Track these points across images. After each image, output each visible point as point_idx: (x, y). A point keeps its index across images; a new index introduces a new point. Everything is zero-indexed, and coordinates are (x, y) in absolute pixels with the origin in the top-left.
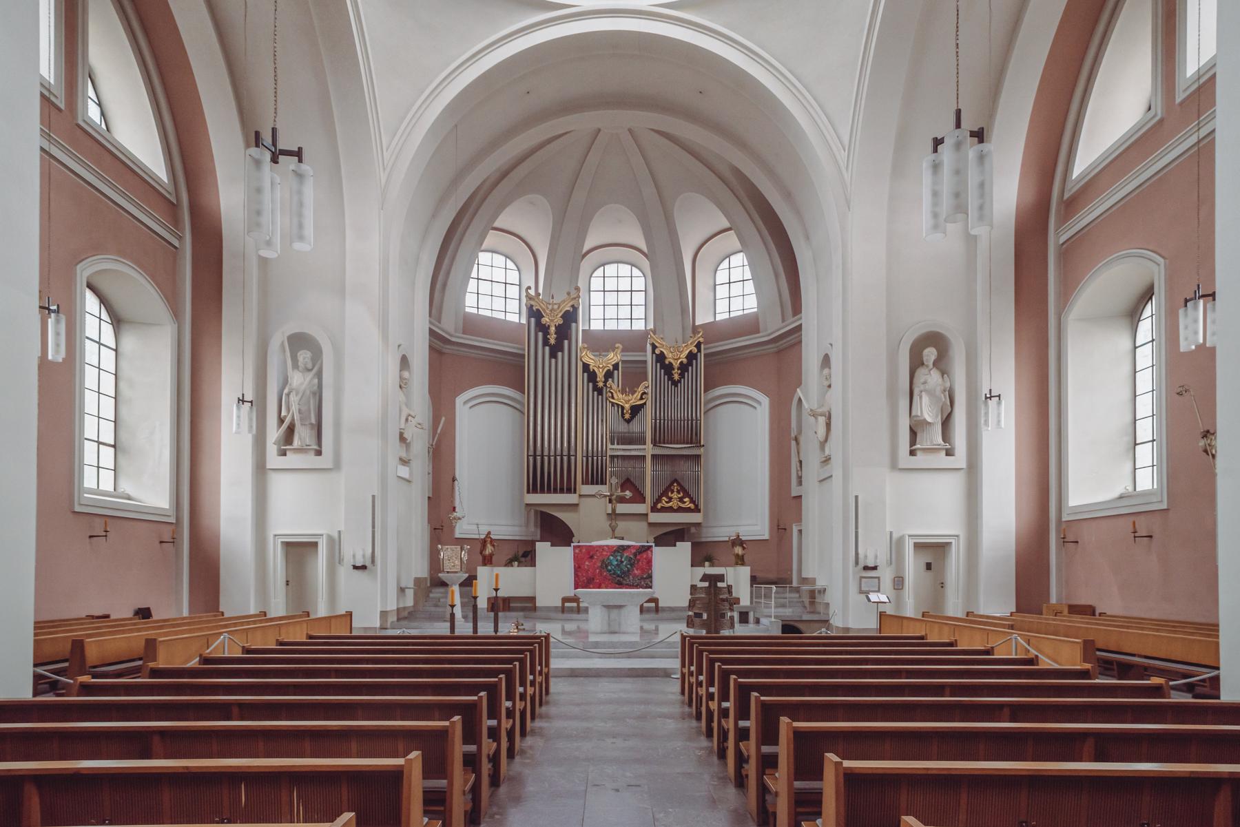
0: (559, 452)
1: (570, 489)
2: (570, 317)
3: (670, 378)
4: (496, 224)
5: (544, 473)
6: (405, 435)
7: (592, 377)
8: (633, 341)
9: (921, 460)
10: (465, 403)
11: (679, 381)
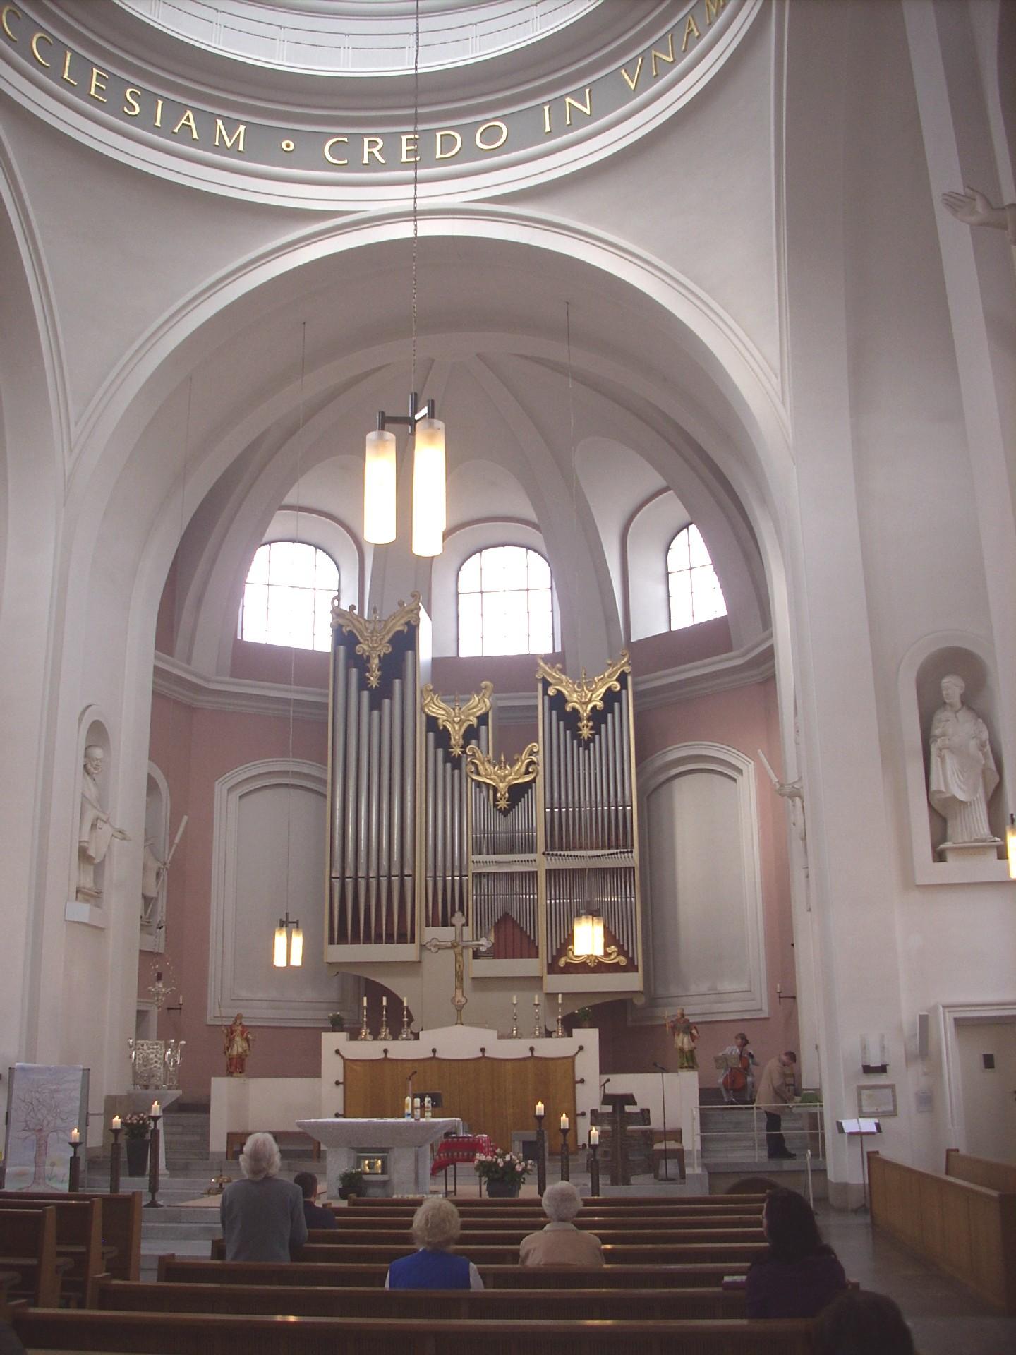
0: (384, 871)
1: (404, 937)
2: (406, 640)
3: (576, 735)
4: (289, 499)
5: (359, 911)
6: (92, 852)
7: (442, 738)
8: (513, 673)
9: (953, 869)
10: (230, 790)
11: (592, 740)
